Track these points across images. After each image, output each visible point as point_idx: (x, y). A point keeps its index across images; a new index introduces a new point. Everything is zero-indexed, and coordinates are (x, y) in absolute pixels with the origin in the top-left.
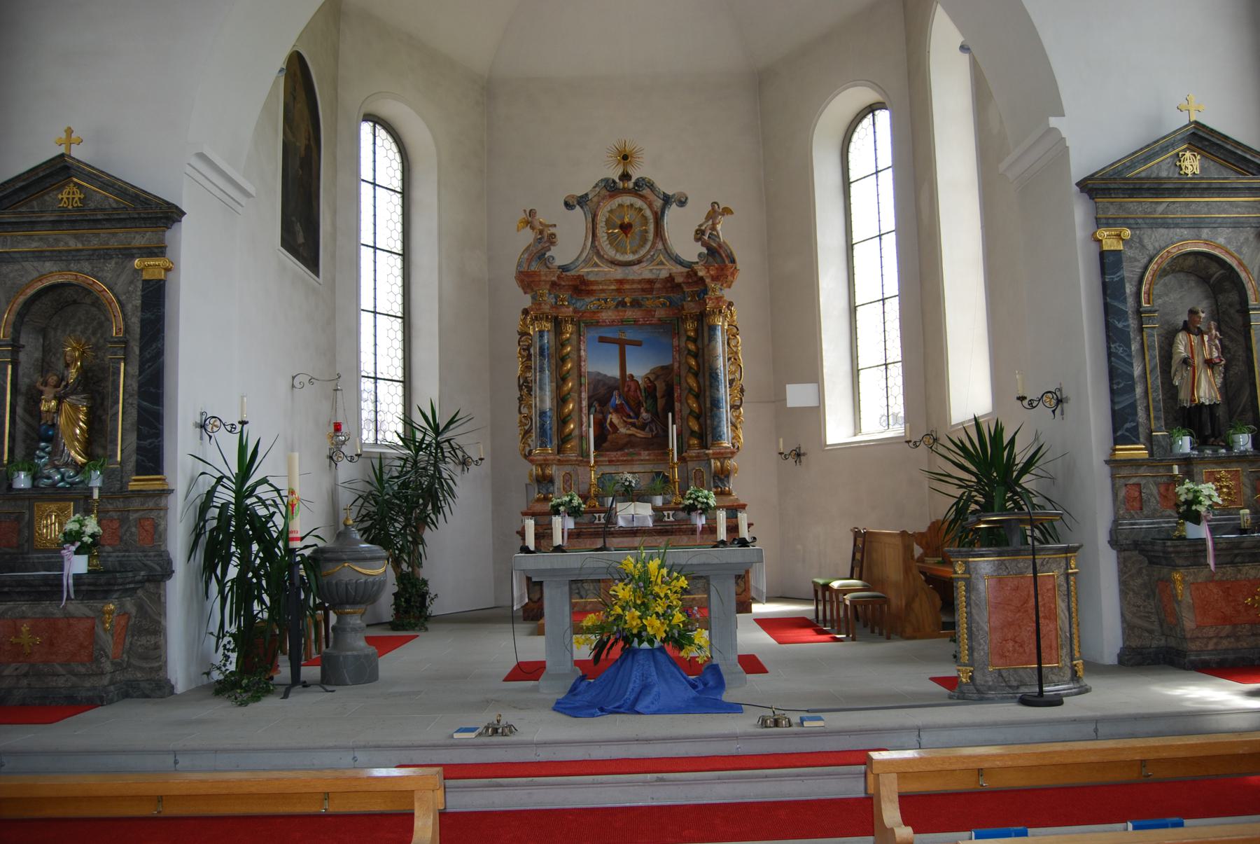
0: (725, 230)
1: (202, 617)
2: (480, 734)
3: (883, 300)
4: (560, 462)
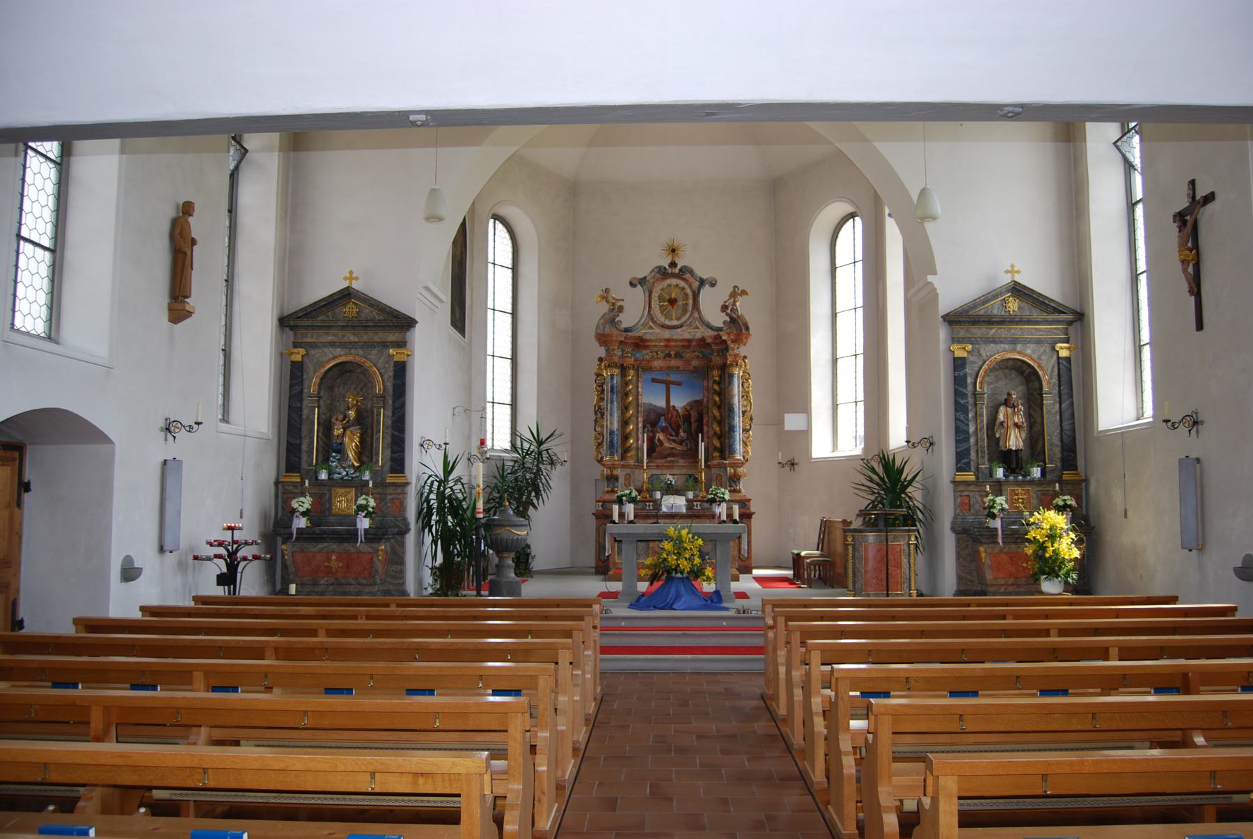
0: (741, 306)
3: (856, 355)
4: (623, 466)
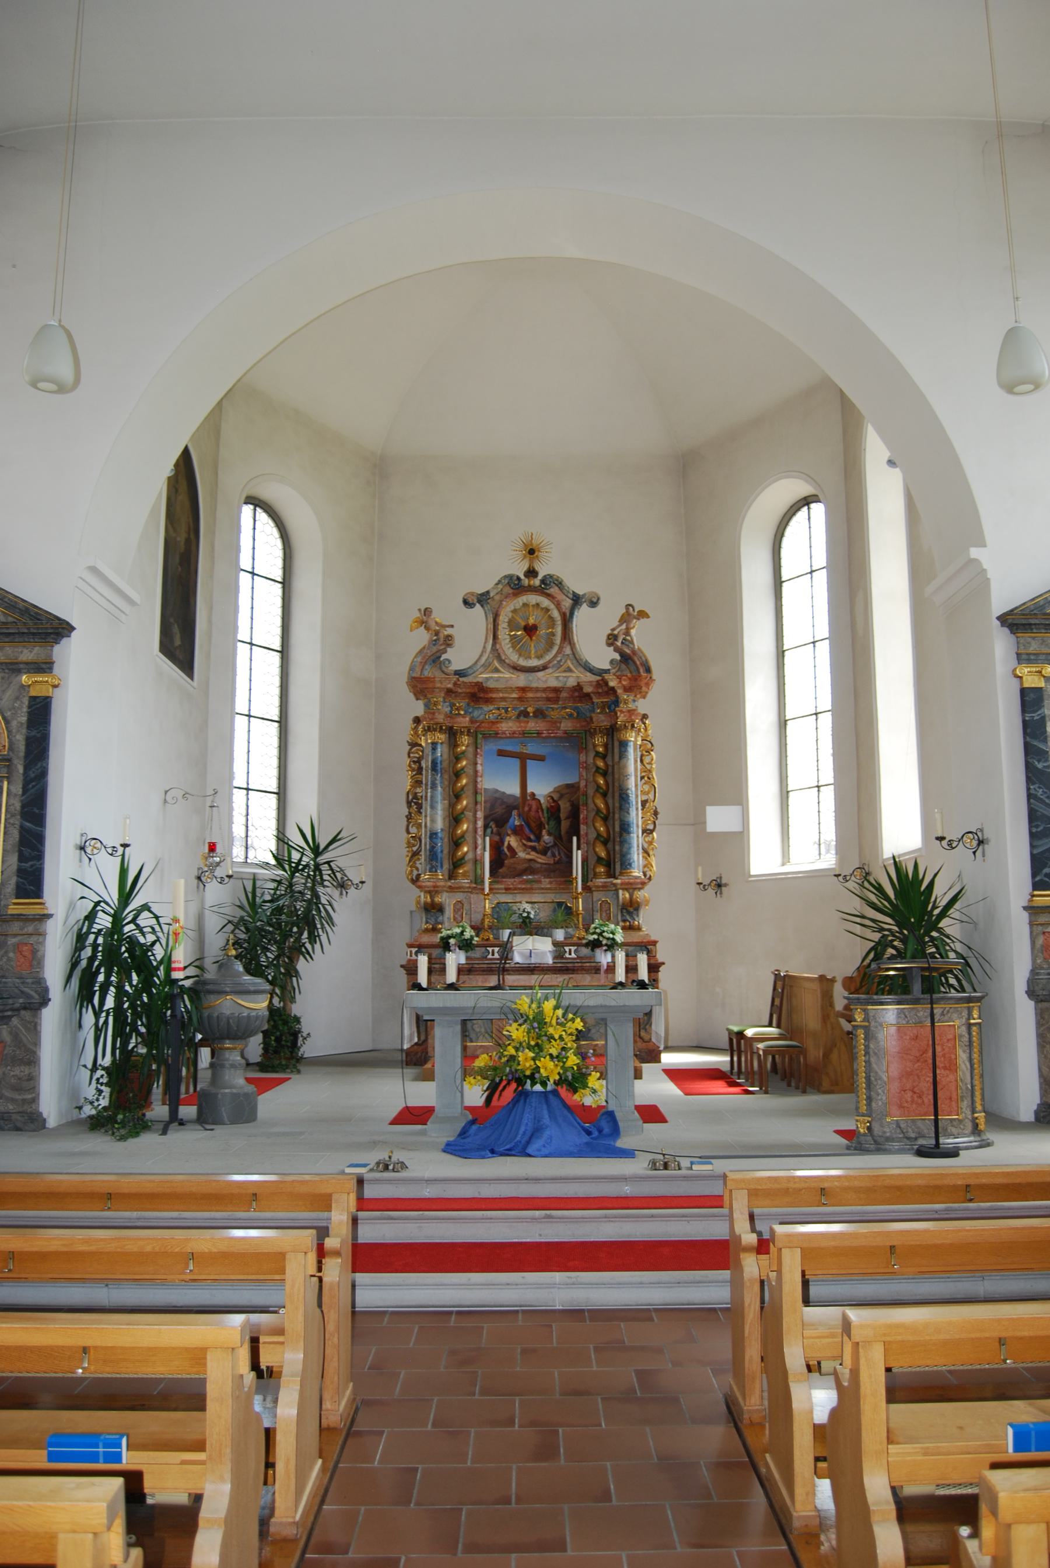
0: (640, 636)
1: (74, 1049)
2: (371, 1170)
4: (452, 889)
